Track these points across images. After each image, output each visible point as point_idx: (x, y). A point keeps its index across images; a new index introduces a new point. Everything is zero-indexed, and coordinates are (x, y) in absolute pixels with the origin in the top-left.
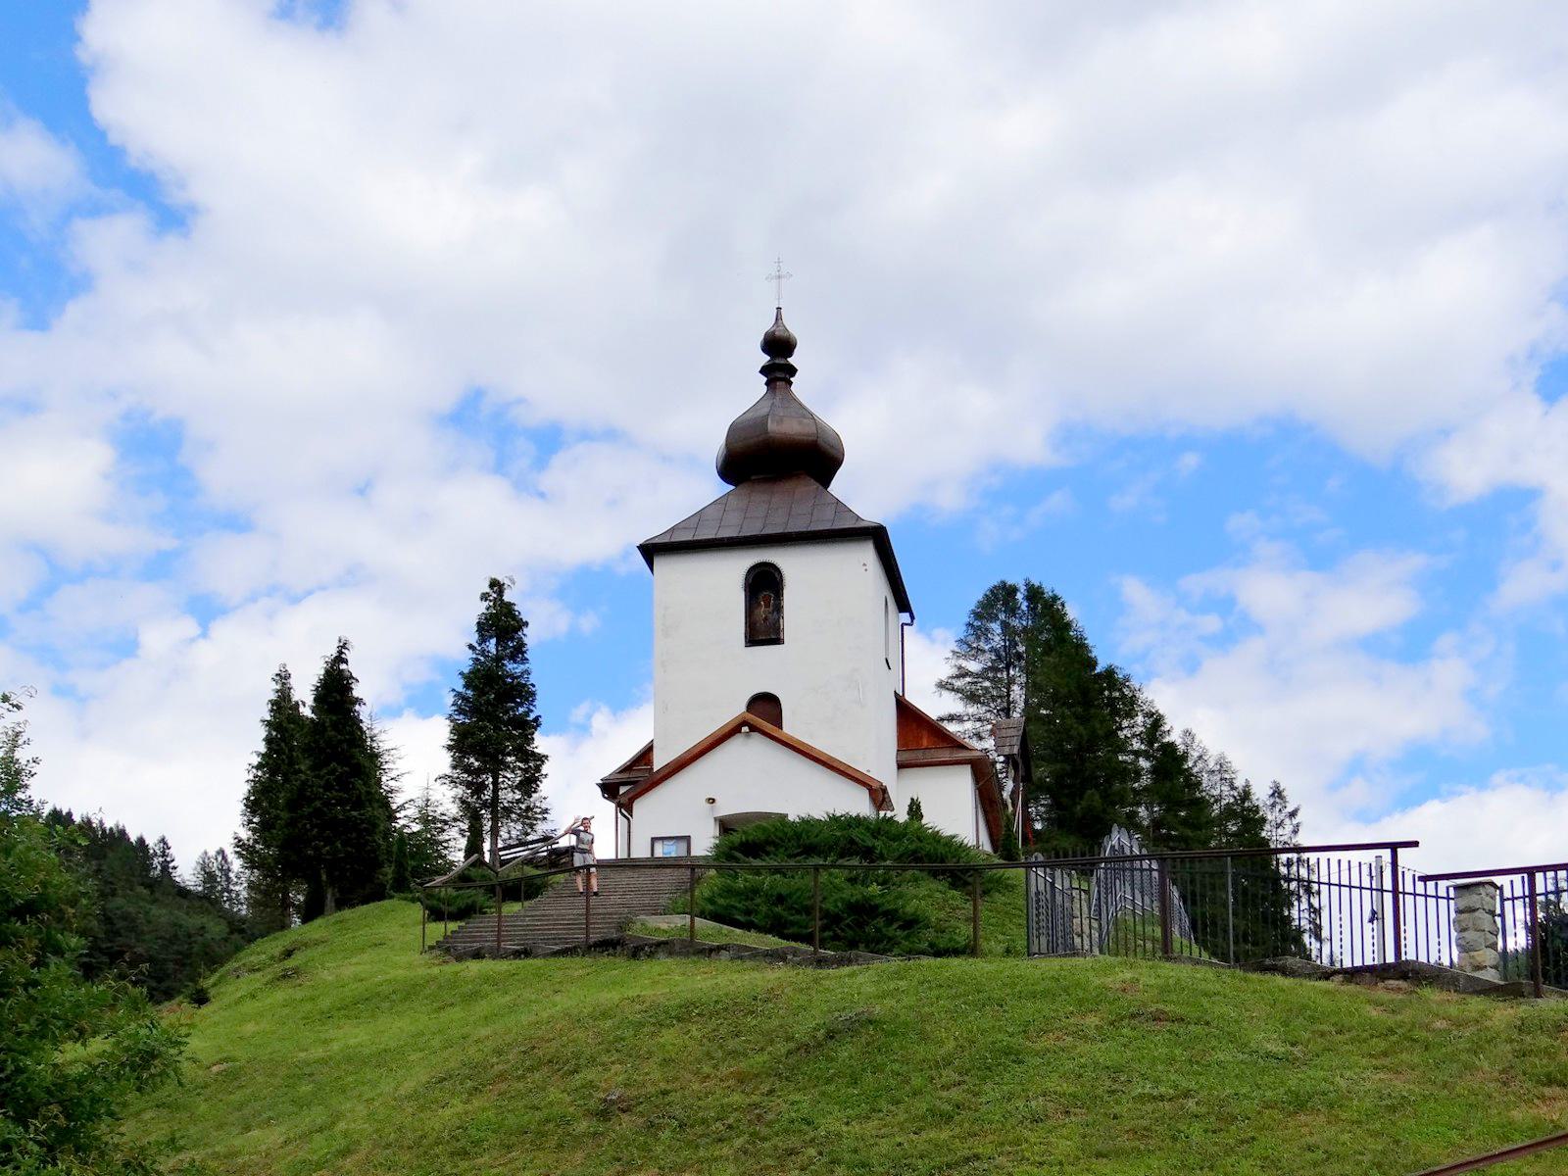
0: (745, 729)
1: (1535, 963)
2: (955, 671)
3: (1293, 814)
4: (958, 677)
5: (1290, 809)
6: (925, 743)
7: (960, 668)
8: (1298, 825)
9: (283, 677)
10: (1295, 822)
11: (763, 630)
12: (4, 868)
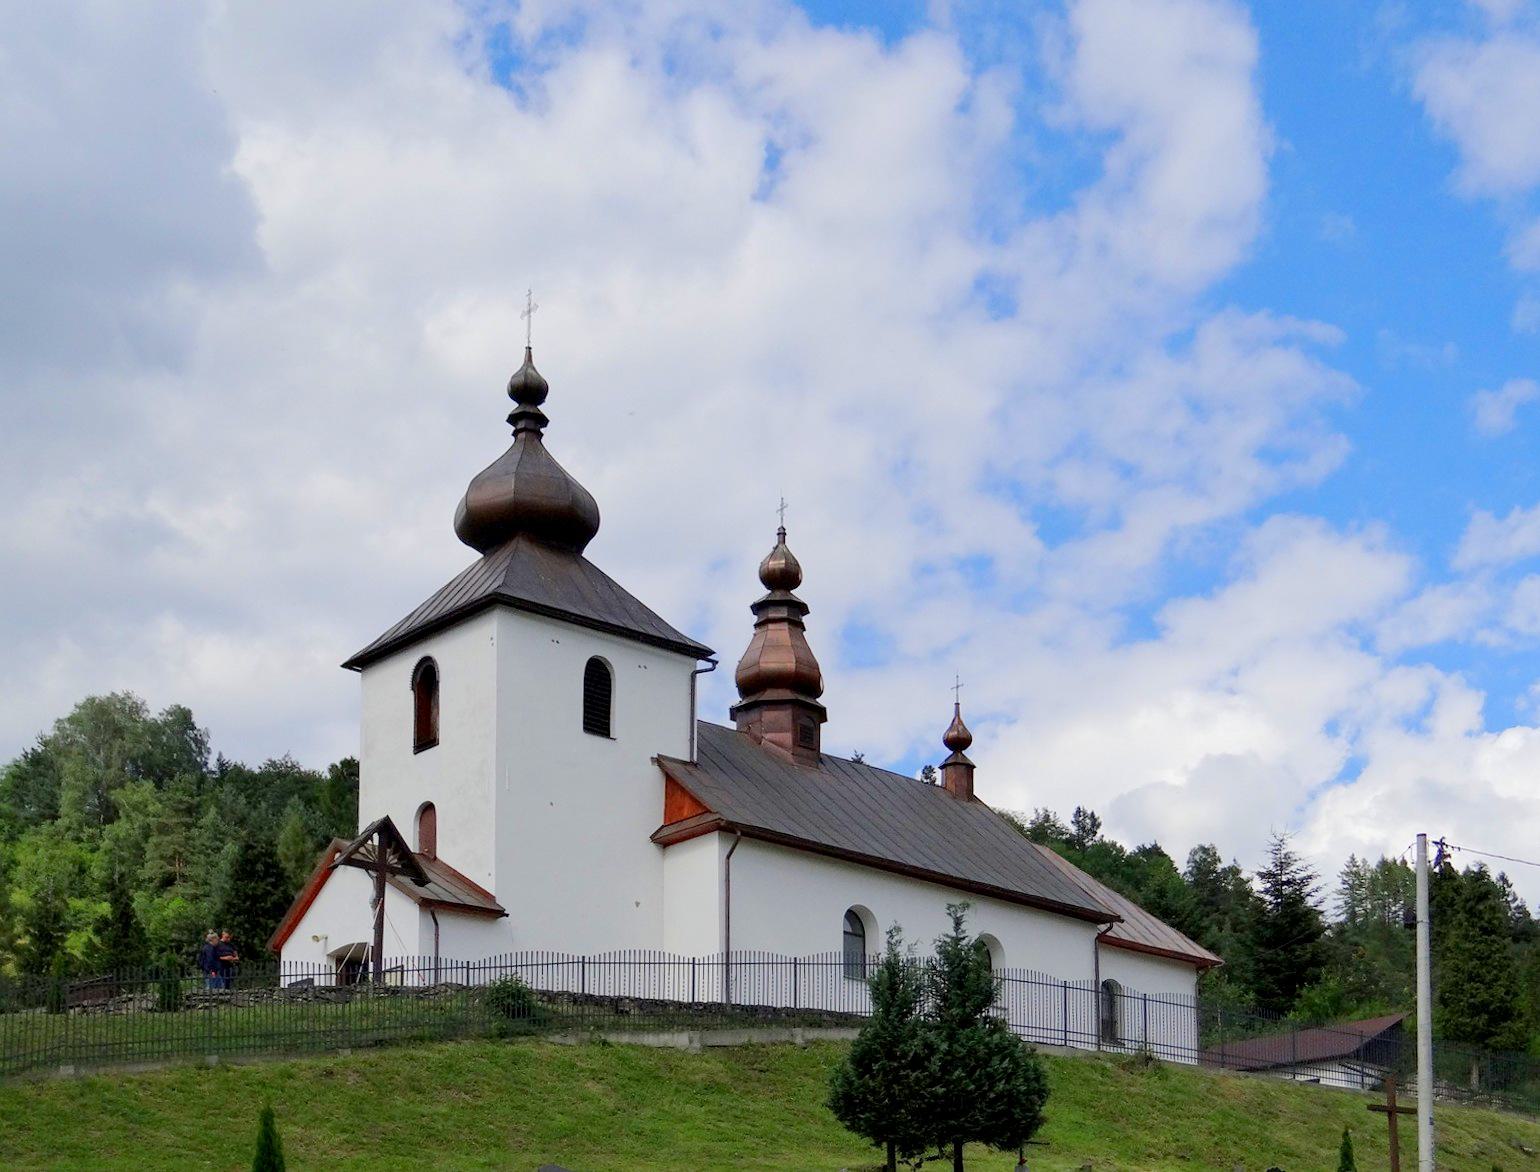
9: (659, 761)
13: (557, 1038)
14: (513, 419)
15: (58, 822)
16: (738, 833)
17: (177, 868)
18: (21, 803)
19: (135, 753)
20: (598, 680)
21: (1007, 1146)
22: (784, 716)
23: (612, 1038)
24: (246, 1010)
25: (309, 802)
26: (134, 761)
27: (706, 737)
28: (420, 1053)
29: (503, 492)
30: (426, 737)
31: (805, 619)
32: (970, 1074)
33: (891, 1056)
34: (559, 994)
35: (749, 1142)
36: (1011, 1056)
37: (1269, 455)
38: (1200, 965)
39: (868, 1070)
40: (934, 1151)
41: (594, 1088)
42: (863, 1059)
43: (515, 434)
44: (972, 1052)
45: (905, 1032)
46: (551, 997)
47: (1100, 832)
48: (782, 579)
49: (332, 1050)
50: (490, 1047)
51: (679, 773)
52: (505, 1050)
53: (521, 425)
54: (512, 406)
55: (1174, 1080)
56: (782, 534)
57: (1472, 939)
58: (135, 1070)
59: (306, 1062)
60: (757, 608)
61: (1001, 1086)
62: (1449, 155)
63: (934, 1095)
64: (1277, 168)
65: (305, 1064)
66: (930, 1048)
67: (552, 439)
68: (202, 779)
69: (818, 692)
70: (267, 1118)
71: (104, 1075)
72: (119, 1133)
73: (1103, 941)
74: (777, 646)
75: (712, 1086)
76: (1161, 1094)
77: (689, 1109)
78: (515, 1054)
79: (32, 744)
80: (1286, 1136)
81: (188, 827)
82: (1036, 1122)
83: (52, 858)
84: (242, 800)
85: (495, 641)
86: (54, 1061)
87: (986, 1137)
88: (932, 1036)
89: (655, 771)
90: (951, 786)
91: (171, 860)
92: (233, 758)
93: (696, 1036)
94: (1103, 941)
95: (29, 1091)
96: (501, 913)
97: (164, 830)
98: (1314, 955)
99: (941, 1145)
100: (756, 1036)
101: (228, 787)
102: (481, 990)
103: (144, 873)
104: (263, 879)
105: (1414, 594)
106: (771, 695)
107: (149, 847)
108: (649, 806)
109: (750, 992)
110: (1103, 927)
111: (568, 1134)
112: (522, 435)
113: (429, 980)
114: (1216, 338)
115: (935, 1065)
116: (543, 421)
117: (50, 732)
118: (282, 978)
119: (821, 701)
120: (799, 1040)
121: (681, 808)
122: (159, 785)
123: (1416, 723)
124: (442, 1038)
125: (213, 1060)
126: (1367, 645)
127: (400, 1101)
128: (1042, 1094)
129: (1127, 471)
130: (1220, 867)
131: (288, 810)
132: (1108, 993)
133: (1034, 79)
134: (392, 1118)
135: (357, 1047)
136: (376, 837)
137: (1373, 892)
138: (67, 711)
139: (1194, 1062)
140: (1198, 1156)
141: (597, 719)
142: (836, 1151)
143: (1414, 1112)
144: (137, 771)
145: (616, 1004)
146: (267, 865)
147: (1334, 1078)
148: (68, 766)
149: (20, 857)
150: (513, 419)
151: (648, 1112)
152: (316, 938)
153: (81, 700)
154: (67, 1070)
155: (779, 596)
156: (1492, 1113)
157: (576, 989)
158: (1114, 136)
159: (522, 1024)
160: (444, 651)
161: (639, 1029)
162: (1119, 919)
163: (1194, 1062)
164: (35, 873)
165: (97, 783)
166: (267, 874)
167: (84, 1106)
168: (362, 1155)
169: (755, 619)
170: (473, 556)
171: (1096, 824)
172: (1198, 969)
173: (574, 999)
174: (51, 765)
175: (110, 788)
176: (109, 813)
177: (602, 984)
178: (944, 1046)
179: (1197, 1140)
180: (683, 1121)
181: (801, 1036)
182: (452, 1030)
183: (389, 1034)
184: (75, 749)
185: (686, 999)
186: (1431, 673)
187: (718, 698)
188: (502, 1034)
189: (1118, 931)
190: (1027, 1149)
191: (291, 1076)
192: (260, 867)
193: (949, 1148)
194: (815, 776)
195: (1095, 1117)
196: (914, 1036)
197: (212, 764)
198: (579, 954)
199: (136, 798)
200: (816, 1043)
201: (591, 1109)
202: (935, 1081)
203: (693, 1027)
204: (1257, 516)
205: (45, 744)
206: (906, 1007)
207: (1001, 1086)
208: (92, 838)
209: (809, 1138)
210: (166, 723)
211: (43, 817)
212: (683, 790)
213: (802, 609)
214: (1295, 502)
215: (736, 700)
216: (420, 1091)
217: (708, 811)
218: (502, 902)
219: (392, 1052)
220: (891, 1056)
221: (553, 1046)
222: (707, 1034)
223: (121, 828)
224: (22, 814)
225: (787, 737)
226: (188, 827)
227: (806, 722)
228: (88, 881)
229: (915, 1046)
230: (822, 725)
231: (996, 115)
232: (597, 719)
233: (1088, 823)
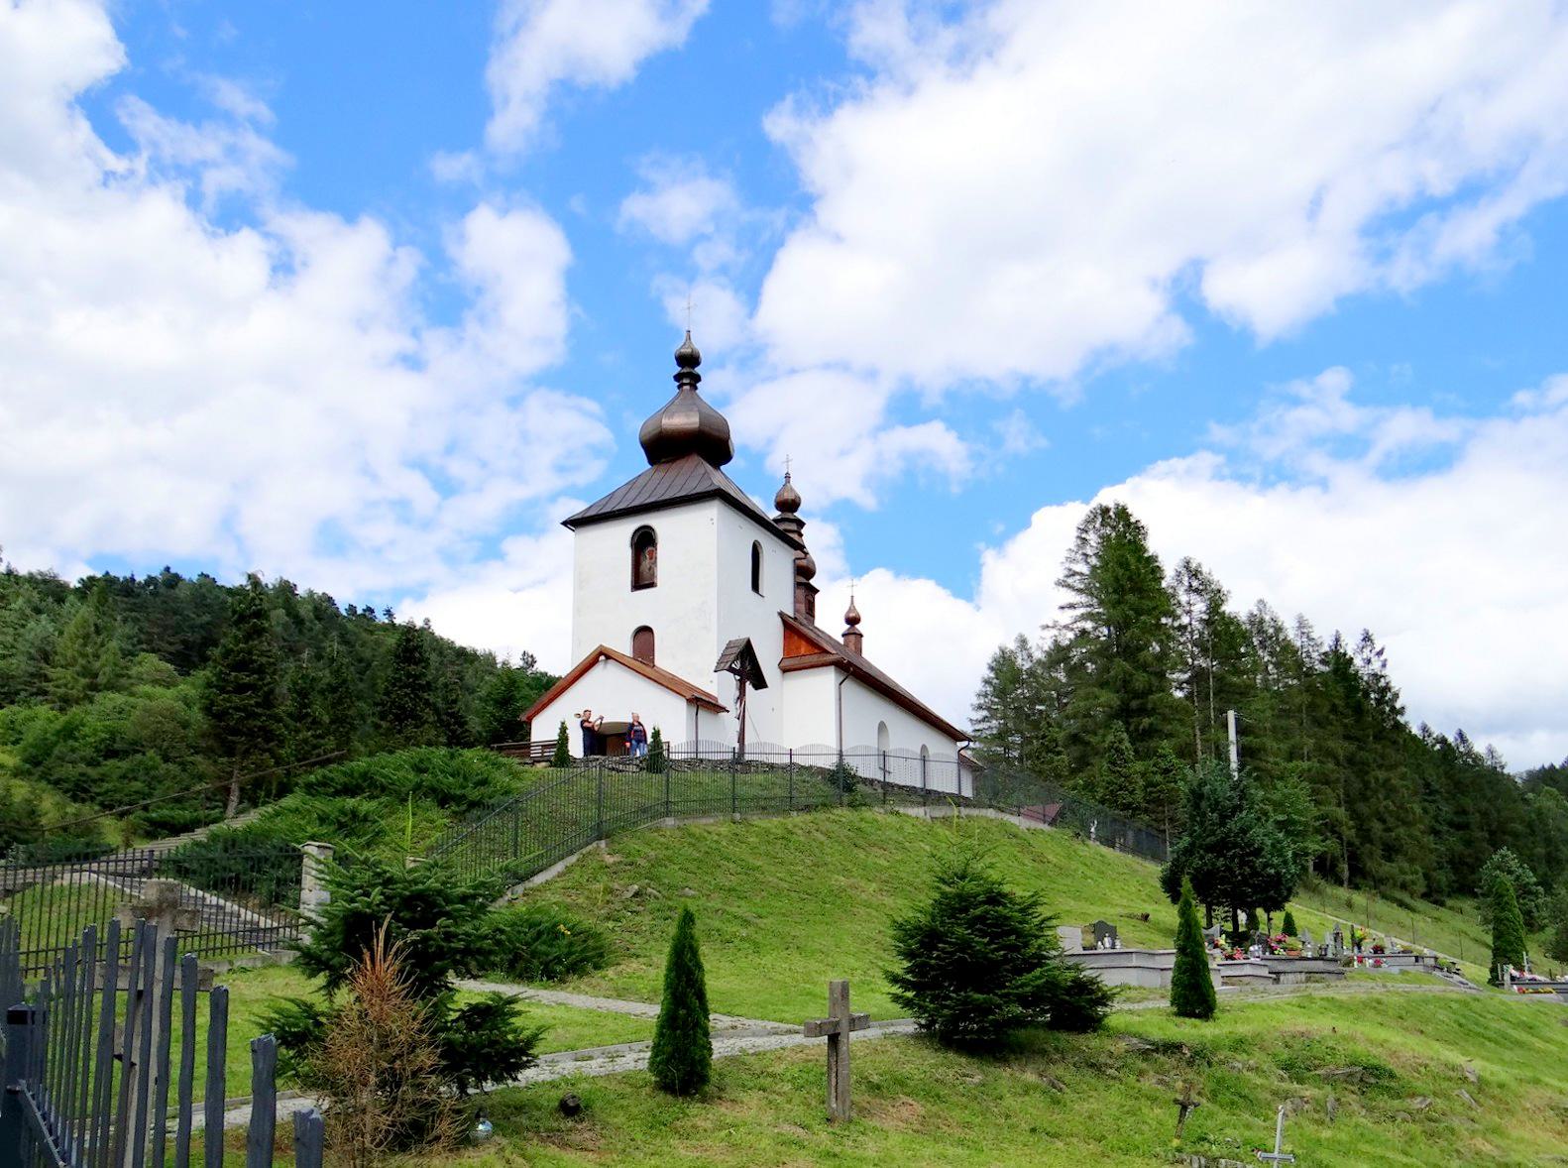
0: (602, 658)
1: (509, 748)
2: (1066, 572)
3: (1380, 653)
4: (1067, 576)
5: (1378, 649)
6: (803, 651)
7: (1070, 570)
8: (1386, 660)
9: (781, 614)
10: (1382, 658)
11: (642, 580)
12: (1455, 1164)
14: (678, 377)
23: (902, 810)
37: (560, 469)
43: (679, 387)
47: (536, 666)
85: (715, 521)
89: (779, 620)
114: (535, 403)
116: (697, 378)
118: (700, 756)
121: (798, 648)
129: (484, 465)
158: (479, 291)
171: (534, 662)
183: (812, 801)
213: (801, 524)
230: (219, 583)
231: (408, 264)
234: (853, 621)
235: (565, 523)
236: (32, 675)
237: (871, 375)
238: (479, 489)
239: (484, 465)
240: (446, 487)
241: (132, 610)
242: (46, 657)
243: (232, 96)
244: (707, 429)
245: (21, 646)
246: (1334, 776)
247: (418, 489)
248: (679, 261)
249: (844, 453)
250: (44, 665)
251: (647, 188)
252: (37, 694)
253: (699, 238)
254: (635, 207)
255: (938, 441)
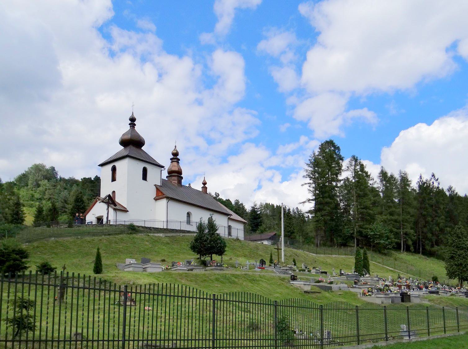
5: (437, 179)
9: (155, 185)
13: (140, 234)
14: (130, 124)
15: (28, 187)
16: (170, 199)
17: (52, 196)
18: (20, 183)
19: (44, 174)
20: (145, 171)
21: (219, 255)
22: (176, 178)
23: (150, 234)
24: (83, 228)
25: (77, 185)
26: (43, 176)
27: (163, 181)
28: (117, 236)
29: (128, 137)
30: (114, 179)
31: (179, 161)
32: (214, 243)
33: (201, 240)
34: (140, 226)
35: (175, 253)
36: (221, 240)
37: (245, 133)
38: (244, 223)
39: (197, 242)
40: (208, 256)
41: (147, 243)
42: (196, 240)
44: (214, 239)
45: (203, 235)
46: (138, 227)
47: (219, 196)
48: (176, 154)
49: (101, 236)
50: (129, 236)
51: (159, 187)
52: (131, 236)
53: (131, 125)
54: (130, 122)
55: (242, 243)
56: (176, 147)
57: (288, 220)
58: (66, 239)
59: (96, 238)
60: (171, 159)
61: (219, 245)
62: (276, 85)
63: (208, 246)
64: (247, 84)
65: (96, 238)
66: (207, 238)
67: (136, 128)
68: (57, 180)
69: (181, 174)
70: (98, 249)
71: (60, 240)
72: (64, 250)
73: (229, 219)
74: (175, 166)
75: (168, 244)
76: (240, 245)
77: (164, 247)
78: (133, 237)
79: (23, 172)
80: (261, 253)
81: (54, 189)
82: (225, 251)
83: (27, 194)
84: (65, 184)
86: (50, 237)
87: (216, 253)
88: (208, 236)
89: (154, 188)
90: (203, 191)
91: (51, 195)
92: (63, 176)
93: (164, 234)
94: (229, 219)
95: (46, 242)
96: (128, 211)
97: (49, 189)
98: (260, 221)
99: (209, 255)
100: (174, 234)
101: (62, 182)
102: (127, 226)
103: (45, 197)
104: (80, 202)
105: (270, 157)
106: (173, 174)
107: (47, 192)
108: (153, 193)
109: (171, 227)
110: (229, 216)
111: (144, 251)
112: (131, 127)
113: (115, 224)
115: (208, 241)
116: (135, 125)
117: (27, 170)
119: (182, 176)
120: (181, 235)
122: (48, 181)
123: (271, 180)
124: (120, 234)
125: (79, 237)
126: (262, 165)
127: (114, 245)
128: (225, 246)
129: (222, 133)
130: (239, 203)
131: (73, 186)
132: (230, 227)
133: (206, 66)
134: (112, 248)
135: (105, 235)
136: (108, 198)
137: (264, 208)
138: (30, 166)
139: (243, 240)
140: (247, 256)
141: (145, 177)
142: (189, 255)
143: (281, 249)
144: (44, 178)
145: (150, 228)
146: (81, 200)
147: (265, 242)
148: (30, 177)
149: (20, 193)
150: (130, 124)
151: (157, 248)
152: (93, 214)
153: (33, 164)
154: (53, 239)
155: (175, 157)
156: (291, 249)
157: (143, 225)
158: (219, 77)
159: (134, 232)
160: (117, 164)
161: (154, 233)
162: (232, 215)
163: (243, 240)
164: (24, 196)
165: (36, 180)
166: (81, 202)
167: (56, 245)
168: (108, 255)
169: (171, 161)
170: (122, 148)
171: (219, 195)
172: (244, 224)
173: (142, 227)
174: (27, 176)
175: (39, 181)
176: (39, 186)
177: (148, 225)
178: (210, 238)
179: (247, 253)
180: (162, 249)
181: (181, 234)
182: (121, 232)
184: (32, 173)
185: (162, 227)
186: (274, 171)
187: (165, 174)
188: (131, 233)
189: (232, 217)
190: (223, 256)
191: (94, 240)
192: (80, 200)
193: (210, 255)
194: (181, 189)
195: (231, 249)
196: (205, 236)
197: (59, 177)
198: (144, 220)
199: (44, 183)
200: (184, 236)
201: (146, 247)
202: (208, 244)
203: (163, 233)
204: (244, 143)
205: (26, 172)
206: (203, 231)
207: (219, 245)
208: (35, 190)
209: (184, 253)
210: (50, 169)
211: (26, 186)
212: (160, 191)
213: (179, 160)
214: (250, 141)
215: (167, 175)
216: (117, 243)
217: (164, 194)
218: (128, 209)
219: (111, 236)
220: (201, 240)
221: (139, 236)
222: (166, 234)
223: (41, 188)
224: (21, 185)
225: (176, 182)
226: (54, 189)
227: (179, 179)
228: (34, 198)
229: (205, 238)
232: (145, 177)
233: (217, 195)
234: (205, 184)
235: (99, 166)
236: (62, 207)
237: (342, 94)
238: (220, 142)
239: (222, 133)
240: (210, 142)
241: (92, 187)
242: (66, 202)
243: (145, 23)
244: (133, 138)
245: (60, 199)
246: (410, 220)
247: (201, 143)
248: (276, 62)
249: (334, 119)
250: (66, 204)
251: (266, 38)
252: (63, 212)
253: (283, 53)
254: (262, 45)
255: (367, 114)
